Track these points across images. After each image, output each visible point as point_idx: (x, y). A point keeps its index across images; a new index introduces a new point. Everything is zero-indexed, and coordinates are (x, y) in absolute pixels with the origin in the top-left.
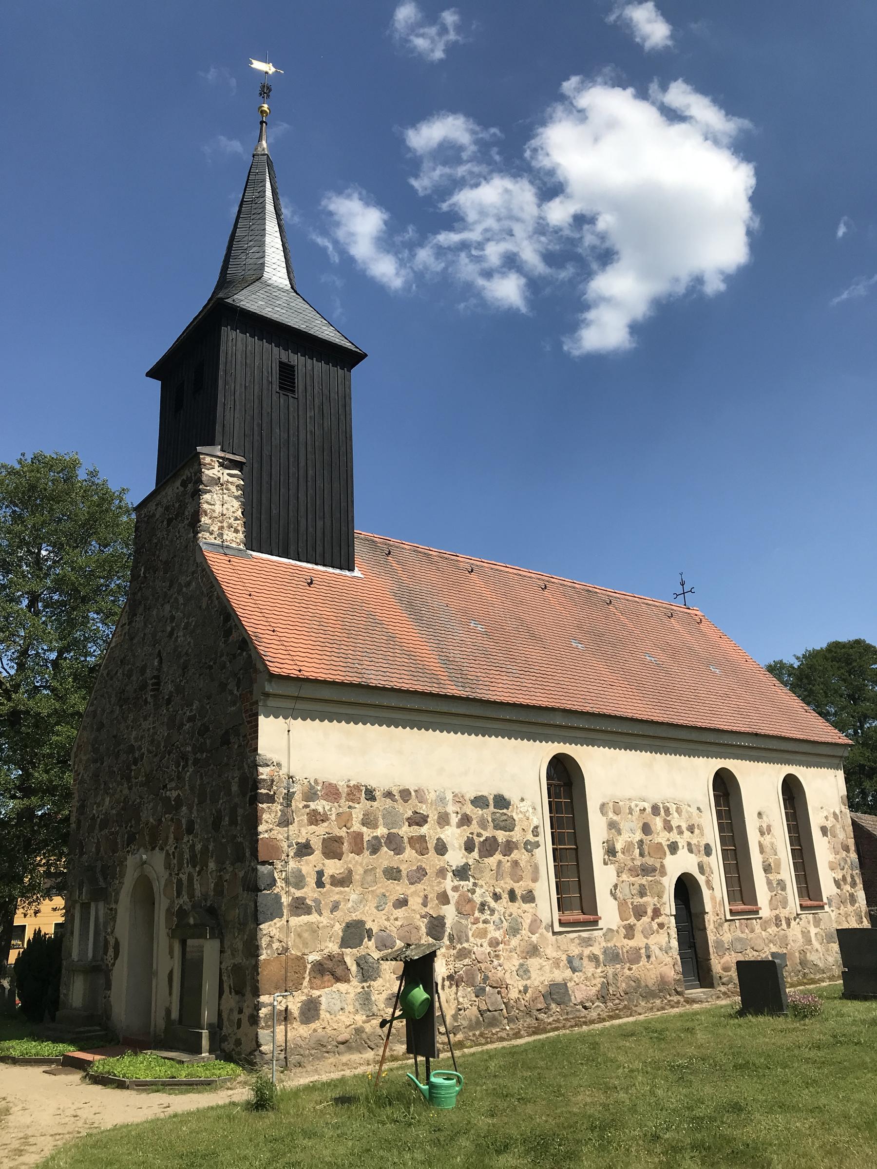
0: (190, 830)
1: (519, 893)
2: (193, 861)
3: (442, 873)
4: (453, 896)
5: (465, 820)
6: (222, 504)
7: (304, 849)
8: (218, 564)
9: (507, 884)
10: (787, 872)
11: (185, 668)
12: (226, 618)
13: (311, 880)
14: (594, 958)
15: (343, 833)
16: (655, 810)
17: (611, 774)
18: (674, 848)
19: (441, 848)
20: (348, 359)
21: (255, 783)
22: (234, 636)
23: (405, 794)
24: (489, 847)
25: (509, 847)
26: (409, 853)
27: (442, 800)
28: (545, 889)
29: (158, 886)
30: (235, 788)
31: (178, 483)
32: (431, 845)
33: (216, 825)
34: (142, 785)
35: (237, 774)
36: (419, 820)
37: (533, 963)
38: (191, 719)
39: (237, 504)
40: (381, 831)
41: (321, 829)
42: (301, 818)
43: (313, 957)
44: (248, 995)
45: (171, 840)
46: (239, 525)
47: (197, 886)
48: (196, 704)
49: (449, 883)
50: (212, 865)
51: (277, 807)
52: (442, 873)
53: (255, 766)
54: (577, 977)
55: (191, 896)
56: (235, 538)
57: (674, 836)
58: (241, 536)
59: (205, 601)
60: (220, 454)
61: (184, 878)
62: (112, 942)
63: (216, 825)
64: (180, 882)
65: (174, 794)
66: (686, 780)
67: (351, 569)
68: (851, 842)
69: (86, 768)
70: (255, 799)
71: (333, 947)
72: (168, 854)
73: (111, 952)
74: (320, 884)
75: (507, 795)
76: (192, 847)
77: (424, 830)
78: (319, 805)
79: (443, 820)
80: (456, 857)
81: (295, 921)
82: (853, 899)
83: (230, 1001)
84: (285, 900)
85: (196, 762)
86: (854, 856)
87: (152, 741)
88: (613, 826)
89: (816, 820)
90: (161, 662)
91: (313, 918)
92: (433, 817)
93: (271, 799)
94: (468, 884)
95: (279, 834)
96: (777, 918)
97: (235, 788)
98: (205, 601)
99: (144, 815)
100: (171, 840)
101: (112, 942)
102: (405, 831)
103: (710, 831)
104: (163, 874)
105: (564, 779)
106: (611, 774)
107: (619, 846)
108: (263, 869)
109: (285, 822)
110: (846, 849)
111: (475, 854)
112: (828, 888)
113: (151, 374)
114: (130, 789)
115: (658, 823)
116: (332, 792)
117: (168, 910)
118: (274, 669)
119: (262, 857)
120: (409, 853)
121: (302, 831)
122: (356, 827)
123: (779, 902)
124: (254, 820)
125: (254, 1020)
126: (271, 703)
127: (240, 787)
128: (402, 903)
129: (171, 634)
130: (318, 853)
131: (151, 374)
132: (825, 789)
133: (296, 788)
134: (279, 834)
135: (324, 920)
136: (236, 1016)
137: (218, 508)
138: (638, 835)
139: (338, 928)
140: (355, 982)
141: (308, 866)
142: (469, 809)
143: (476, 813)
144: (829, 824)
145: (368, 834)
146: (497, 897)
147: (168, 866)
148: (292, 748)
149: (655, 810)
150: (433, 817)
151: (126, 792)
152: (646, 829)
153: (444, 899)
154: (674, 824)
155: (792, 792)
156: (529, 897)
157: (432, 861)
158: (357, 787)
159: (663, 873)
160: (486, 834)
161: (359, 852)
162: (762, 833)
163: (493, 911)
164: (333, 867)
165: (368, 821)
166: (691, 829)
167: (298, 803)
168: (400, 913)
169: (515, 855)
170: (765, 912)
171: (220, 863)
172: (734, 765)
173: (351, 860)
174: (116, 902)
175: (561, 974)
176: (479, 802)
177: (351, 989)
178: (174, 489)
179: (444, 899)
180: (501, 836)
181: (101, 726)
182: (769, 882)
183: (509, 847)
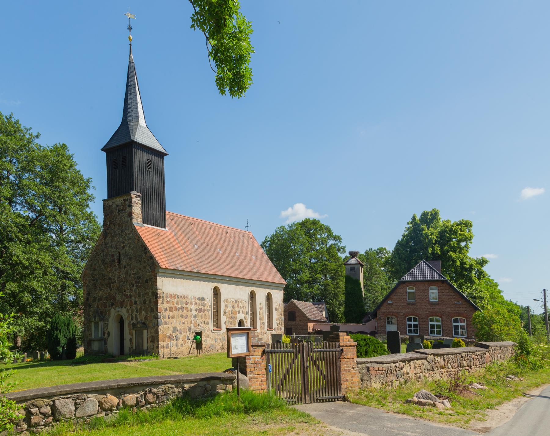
0: (135, 303)
1: (206, 322)
2: (137, 311)
3: (191, 316)
4: (193, 322)
5: (196, 303)
6: (137, 210)
7: (166, 310)
8: (137, 227)
9: (204, 320)
10: (265, 320)
12: (145, 249)
13: (167, 317)
14: (220, 339)
15: (172, 306)
16: (236, 301)
17: (228, 292)
19: (191, 310)
20: (161, 155)
21: (157, 294)
22: (148, 254)
23: (184, 296)
24: (200, 310)
25: (204, 310)
26: (185, 311)
27: (191, 298)
28: (211, 321)
29: (125, 318)
30: (150, 294)
31: (122, 199)
32: (189, 309)
33: (145, 302)
34: (116, 290)
35: (151, 291)
36: (187, 303)
37: (208, 339)
38: (133, 274)
39: (140, 209)
40: (180, 306)
41: (169, 305)
42: (165, 302)
43: (168, 334)
44: (156, 342)
46: (141, 216)
47: (138, 317)
48: (135, 270)
49: (192, 319)
50: (143, 312)
51: (161, 300)
52: (191, 316)
53: (157, 289)
54: (216, 343)
55: (137, 319)
56: (140, 220)
57: (239, 309)
58: (141, 219)
60: (136, 193)
61: (134, 316)
62: (106, 332)
63: (145, 302)
64: (132, 317)
65: (129, 294)
67: (165, 228)
68: (283, 313)
69: (89, 282)
70: (157, 298)
71: (171, 332)
72: (128, 309)
73: (106, 335)
74: (169, 318)
76: (137, 308)
77: (188, 306)
78: (169, 299)
79: (191, 303)
80: (194, 313)
81: (165, 326)
82: (281, 329)
83: (150, 344)
84: (163, 321)
85: (137, 286)
86: (283, 317)
87: (119, 278)
88: (226, 306)
89: (274, 306)
90: (120, 254)
92: (189, 303)
93: (160, 298)
94: (196, 319)
95: (162, 306)
96: (261, 333)
97: (150, 294)
98: (136, 241)
99: (117, 298)
101: (106, 332)
102: (184, 306)
103: (248, 309)
104: (127, 315)
105: (216, 292)
106: (228, 292)
108: (159, 314)
109: (163, 303)
110: (281, 315)
112: (275, 325)
113: (102, 150)
114: (111, 290)
115: (236, 305)
116: (171, 296)
117: (129, 324)
120: (185, 311)
122: (175, 305)
123: (262, 328)
124: (156, 303)
125: (158, 347)
126: (160, 274)
128: (184, 323)
129: (123, 247)
131: (102, 150)
132: (278, 296)
133: (164, 295)
134: (162, 306)
135: (170, 326)
136: (152, 347)
137: (136, 211)
138: (231, 309)
139: (172, 328)
140: (175, 340)
141: (167, 314)
143: (198, 302)
144: (277, 307)
145: (177, 306)
146: (201, 323)
147: (128, 312)
148: (166, 286)
150: (189, 303)
151: (109, 291)
152: (233, 307)
155: (269, 297)
156: (208, 323)
157: (189, 314)
159: (236, 319)
161: (176, 311)
164: (171, 314)
165: (177, 304)
167: (165, 299)
168: (183, 325)
170: (259, 331)
171: (146, 312)
172: (255, 289)
173: (175, 313)
174: (108, 321)
175: (213, 342)
176: (199, 299)
177: (174, 342)
179: (191, 323)
180: (203, 308)
181: (95, 270)
182: (260, 323)
183: (204, 310)
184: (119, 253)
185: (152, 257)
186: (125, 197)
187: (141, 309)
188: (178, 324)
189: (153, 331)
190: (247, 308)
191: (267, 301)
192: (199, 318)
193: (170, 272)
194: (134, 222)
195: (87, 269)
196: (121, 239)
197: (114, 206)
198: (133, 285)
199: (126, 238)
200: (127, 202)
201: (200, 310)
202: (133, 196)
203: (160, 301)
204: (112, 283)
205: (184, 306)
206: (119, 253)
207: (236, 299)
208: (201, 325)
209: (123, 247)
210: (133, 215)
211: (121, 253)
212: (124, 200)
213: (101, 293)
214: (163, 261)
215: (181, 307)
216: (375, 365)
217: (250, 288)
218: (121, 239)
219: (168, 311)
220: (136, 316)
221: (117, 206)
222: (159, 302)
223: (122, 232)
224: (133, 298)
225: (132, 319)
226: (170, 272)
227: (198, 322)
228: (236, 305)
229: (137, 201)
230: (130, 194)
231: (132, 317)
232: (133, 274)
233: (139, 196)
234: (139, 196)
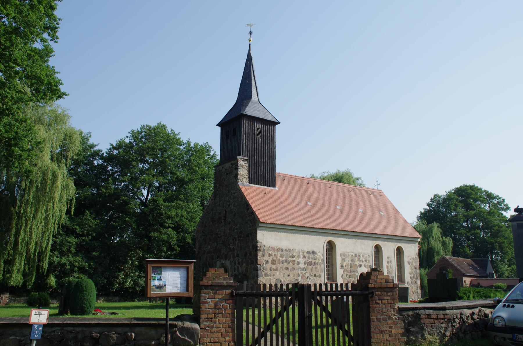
0: (238, 256)
2: (239, 263)
3: (298, 269)
4: (301, 275)
6: (243, 172)
7: (267, 262)
9: (314, 272)
11: (234, 215)
12: (247, 205)
13: (269, 269)
15: (275, 259)
16: (356, 255)
17: (343, 245)
18: (360, 266)
19: (298, 263)
21: (257, 247)
22: (250, 210)
23: (290, 250)
24: (310, 264)
30: (251, 247)
31: (230, 163)
36: (293, 257)
38: (236, 229)
39: (246, 171)
40: (284, 259)
41: (271, 258)
45: (232, 258)
46: (247, 177)
47: (240, 269)
49: (300, 272)
50: (244, 265)
55: (238, 271)
56: (246, 181)
58: (248, 180)
59: (240, 199)
61: (236, 267)
63: (246, 255)
64: (235, 268)
65: (232, 247)
66: (366, 248)
74: (270, 270)
75: (315, 251)
76: (238, 260)
77: (294, 259)
79: (299, 256)
80: (302, 266)
81: (265, 278)
82: (416, 282)
84: (263, 273)
85: (239, 240)
88: (343, 260)
89: (406, 260)
90: (226, 212)
91: (269, 277)
93: (260, 250)
97: (251, 247)
98: (240, 199)
100: (232, 258)
102: (290, 259)
105: (331, 247)
106: (343, 245)
107: (344, 265)
109: (263, 256)
110: (416, 268)
111: (306, 265)
113: (217, 125)
116: (273, 249)
118: (261, 221)
119: (259, 263)
121: (266, 258)
122: (279, 257)
124: (256, 255)
126: (260, 228)
127: (253, 248)
128: (289, 275)
129: (229, 205)
130: (270, 263)
131: (217, 125)
135: (271, 278)
137: (242, 173)
141: (268, 266)
142: (305, 254)
144: (411, 261)
147: (231, 264)
148: (265, 238)
149: (356, 255)
150: (296, 256)
152: (352, 261)
153: (299, 275)
154: (361, 259)
155: (399, 252)
156: (320, 276)
157: (296, 266)
158: (279, 248)
160: (309, 261)
162: (388, 263)
163: (310, 279)
165: (281, 256)
166: (366, 261)
167: (266, 252)
168: (288, 278)
169: (316, 266)
173: (279, 266)
176: (308, 252)
178: (227, 165)
179: (299, 275)
180: (313, 261)
184: (225, 210)
185: (253, 213)
186: (233, 162)
187: (242, 261)
188: (282, 276)
189: (253, 282)
190: (371, 262)
191: (397, 255)
192: (309, 271)
193: (272, 226)
194: (240, 183)
195: (199, 226)
196: (227, 198)
197: (223, 170)
198: (236, 240)
199: (232, 197)
200: (234, 166)
201: (310, 264)
202: (239, 160)
203: (260, 254)
204: (219, 238)
205: (290, 259)
206: (225, 210)
207: (357, 253)
208: (312, 278)
209: (229, 205)
210: (239, 176)
211: (227, 211)
212: (232, 164)
213: (209, 247)
214: (262, 215)
215: (286, 261)
216: (431, 311)
217: (375, 242)
218: (227, 198)
219: (270, 264)
220: (238, 267)
221: (226, 170)
222: (259, 254)
223: (229, 192)
224: (236, 251)
225: (234, 271)
226: (272, 226)
227: (307, 275)
228: (356, 259)
229: (244, 164)
230: (237, 159)
231: (235, 268)
232: (236, 229)
233: (246, 160)
234: (246, 160)
